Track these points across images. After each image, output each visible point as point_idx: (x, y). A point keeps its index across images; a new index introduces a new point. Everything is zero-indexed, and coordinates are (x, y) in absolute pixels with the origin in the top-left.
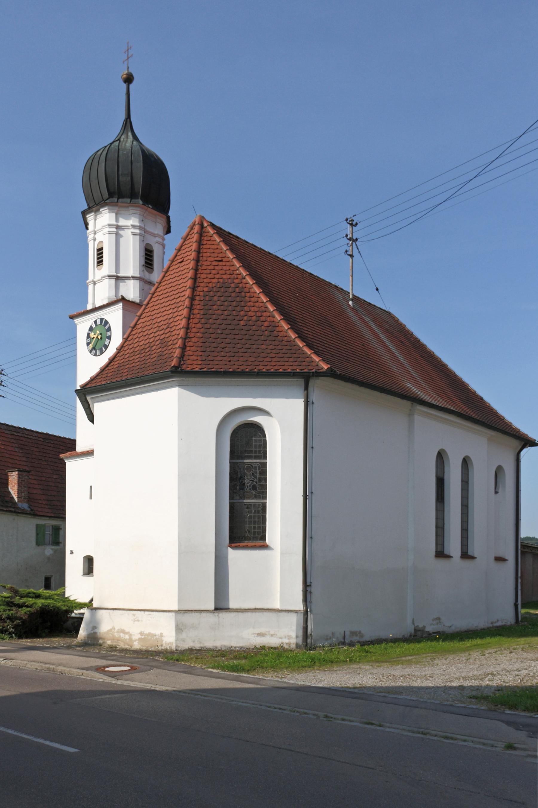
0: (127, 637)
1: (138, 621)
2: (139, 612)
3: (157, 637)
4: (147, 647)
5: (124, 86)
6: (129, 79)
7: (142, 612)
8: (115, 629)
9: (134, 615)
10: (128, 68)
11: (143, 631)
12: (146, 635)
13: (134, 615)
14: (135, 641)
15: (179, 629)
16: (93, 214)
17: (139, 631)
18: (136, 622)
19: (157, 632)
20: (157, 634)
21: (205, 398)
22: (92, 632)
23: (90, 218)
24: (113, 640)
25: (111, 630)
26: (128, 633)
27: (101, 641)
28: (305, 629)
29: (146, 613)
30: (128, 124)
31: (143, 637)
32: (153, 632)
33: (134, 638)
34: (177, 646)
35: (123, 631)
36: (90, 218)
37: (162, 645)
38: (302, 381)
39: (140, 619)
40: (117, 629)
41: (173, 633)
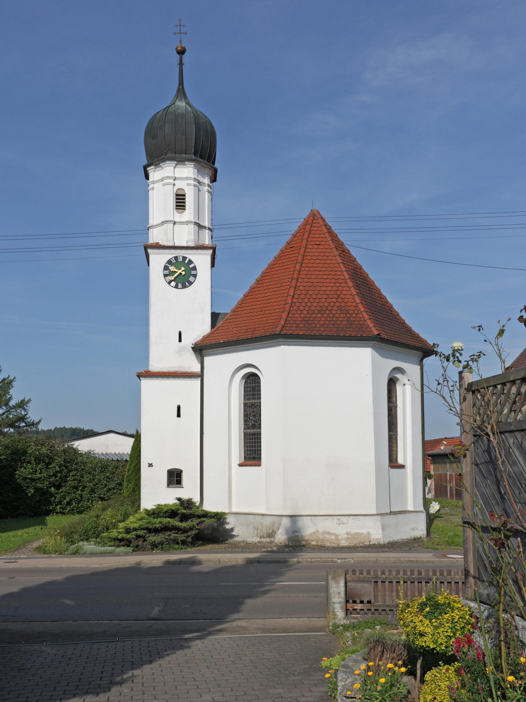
0: (333, 537)
1: (344, 524)
2: (343, 517)
3: (365, 535)
4: (356, 544)
5: (177, 56)
6: (181, 52)
7: (348, 517)
8: (318, 532)
9: (339, 519)
10: (180, 42)
11: (349, 531)
12: (353, 534)
13: (339, 519)
14: (342, 540)
15: (384, 528)
16: (153, 167)
17: (345, 532)
18: (341, 525)
19: (365, 531)
20: (364, 533)
21: (385, 359)
22: (293, 535)
23: (150, 169)
24: (318, 541)
25: (314, 533)
26: (334, 534)
27: (304, 543)
28: (39, 637)
29: (351, 517)
30: (181, 92)
31: (350, 536)
32: (359, 531)
33: (340, 538)
34: (384, 541)
35: (329, 533)
36: (150, 169)
37: (370, 542)
38: (421, 354)
39: (345, 522)
40: (321, 531)
41: (381, 532)
